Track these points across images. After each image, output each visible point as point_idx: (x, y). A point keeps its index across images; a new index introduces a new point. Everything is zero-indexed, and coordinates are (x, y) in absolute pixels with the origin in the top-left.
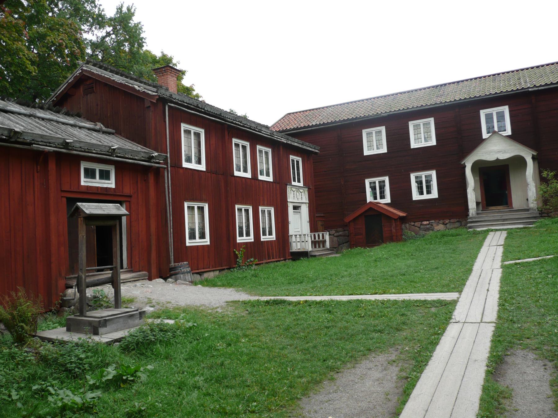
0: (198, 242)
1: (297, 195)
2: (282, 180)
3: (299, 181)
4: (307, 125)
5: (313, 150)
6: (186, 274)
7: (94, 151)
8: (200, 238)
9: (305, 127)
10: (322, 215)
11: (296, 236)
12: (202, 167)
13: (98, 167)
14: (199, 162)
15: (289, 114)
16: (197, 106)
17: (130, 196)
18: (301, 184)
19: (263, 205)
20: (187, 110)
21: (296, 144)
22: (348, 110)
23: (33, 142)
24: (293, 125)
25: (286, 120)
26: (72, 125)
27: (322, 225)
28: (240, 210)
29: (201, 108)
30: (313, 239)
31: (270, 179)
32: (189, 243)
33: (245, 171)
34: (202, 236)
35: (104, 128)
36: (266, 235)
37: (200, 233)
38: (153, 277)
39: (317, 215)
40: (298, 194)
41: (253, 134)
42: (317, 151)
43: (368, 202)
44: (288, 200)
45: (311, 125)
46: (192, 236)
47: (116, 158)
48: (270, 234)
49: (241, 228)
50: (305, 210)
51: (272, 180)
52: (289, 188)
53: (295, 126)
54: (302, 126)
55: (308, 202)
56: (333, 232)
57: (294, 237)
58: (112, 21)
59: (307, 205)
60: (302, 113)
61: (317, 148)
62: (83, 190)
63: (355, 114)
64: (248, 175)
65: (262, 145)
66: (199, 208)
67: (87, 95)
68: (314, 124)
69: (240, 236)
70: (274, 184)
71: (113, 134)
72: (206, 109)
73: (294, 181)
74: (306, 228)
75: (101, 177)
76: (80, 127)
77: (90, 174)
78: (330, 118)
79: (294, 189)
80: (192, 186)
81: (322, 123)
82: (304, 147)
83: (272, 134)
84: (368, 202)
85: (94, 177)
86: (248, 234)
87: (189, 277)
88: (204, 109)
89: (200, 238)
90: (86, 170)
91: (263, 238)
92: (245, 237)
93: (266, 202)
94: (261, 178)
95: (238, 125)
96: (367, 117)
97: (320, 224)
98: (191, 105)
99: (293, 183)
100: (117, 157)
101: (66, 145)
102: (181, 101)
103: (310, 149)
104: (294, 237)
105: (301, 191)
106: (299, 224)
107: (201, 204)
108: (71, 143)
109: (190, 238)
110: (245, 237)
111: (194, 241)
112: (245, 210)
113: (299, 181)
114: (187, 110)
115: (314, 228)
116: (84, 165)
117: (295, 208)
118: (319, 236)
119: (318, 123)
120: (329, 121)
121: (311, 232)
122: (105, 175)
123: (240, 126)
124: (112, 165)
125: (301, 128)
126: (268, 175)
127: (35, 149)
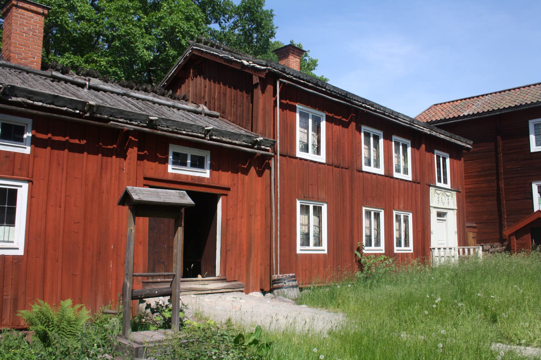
0: (312, 249)
1: (443, 199)
2: (423, 182)
3: (445, 182)
4: (456, 116)
5: (464, 144)
6: (292, 289)
7: (184, 132)
8: (315, 245)
9: (454, 118)
10: (475, 225)
11: (439, 249)
12: (322, 158)
13: (190, 152)
14: (318, 152)
15: (436, 105)
16: (317, 84)
17: (228, 189)
18: (448, 186)
19: (399, 209)
20: (303, 88)
21: (442, 136)
22: (509, 98)
23: (111, 118)
24: (439, 116)
25: (431, 111)
26: (169, 106)
27: (473, 238)
28: (368, 213)
29: (322, 87)
30: (461, 254)
31: (409, 177)
32: (300, 250)
33: (377, 165)
34: (319, 243)
35: (207, 110)
36: (370, 245)
37: (397, 243)
38: (251, 290)
39: (467, 225)
40: (443, 197)
41: (389, 126)
42: (469, 146)
43: (535, 210)
44: (431, 205)
45: (461, 115)
46: (306, 241)
47: (210, 142)
48: (407, 244)
49: (369, 237)
50: (452, 218)
51: (410, 179)
52: (432, 190)
53: (442, 118)
54: (451, 117)
55: (456, 208)
56: (487, 247)
57: (436, 250)
58: (238, 11)
59: (456, 211)
60: (451, 103)
61: (469, 142)
62: (170, 178)
63: (518, 101)
64: (381, 171)
65: (398, 135)
66: (315, 207)
67: (196, 77)
68: (466, 114)
69: (397, 246)
70: (414, 184)
71: (217, 117)
72: (327, 88)
73: (439, 181)
74: (453, 240)
75: (193, 165)
76: (179, 109)
77: (180, 160)
78: (487, 107)
79: (438, 192)
80: (306, 181)
81: (476, 113)
82: (453, 140)
83: (412, 121)
84: (535, 210)
85: (184, 164)
86: (378, 244)
87: (294, 293)
88: (325, 88)
89: (315, 245)
90: (175, 155)
91: (396, 250)
92: (403, 248)
93: (402, 206)
94: (396, 175)
95: (369, 109)
96: (535, 103)
97: (471, 235)
98: (309, 82)
99: (438, 184)
100: (211, 139)
101: (152, 124)
102: (296, 77)
103: (460, 143)
104: (436, 250)
105: (448, 194)
106: (445, 235)
107: (318, 204)
108: (156, 120)
109: (302, 245)
110: (373, 247)
111: (307, 248)
112: (375, 214)
113: (445, 182)
114: (303, 88)
115: (463, 241)
116: (173, 149)
117: (440, 215)
118: (469, 250)
119: (471, 113)
120: (485, 110)
121: (459, 245)
122: (198, 163)
123: (371, 110)
124: (207, 150)
125: (450, 119)
126: (406, 172)
127: (113, 126)
